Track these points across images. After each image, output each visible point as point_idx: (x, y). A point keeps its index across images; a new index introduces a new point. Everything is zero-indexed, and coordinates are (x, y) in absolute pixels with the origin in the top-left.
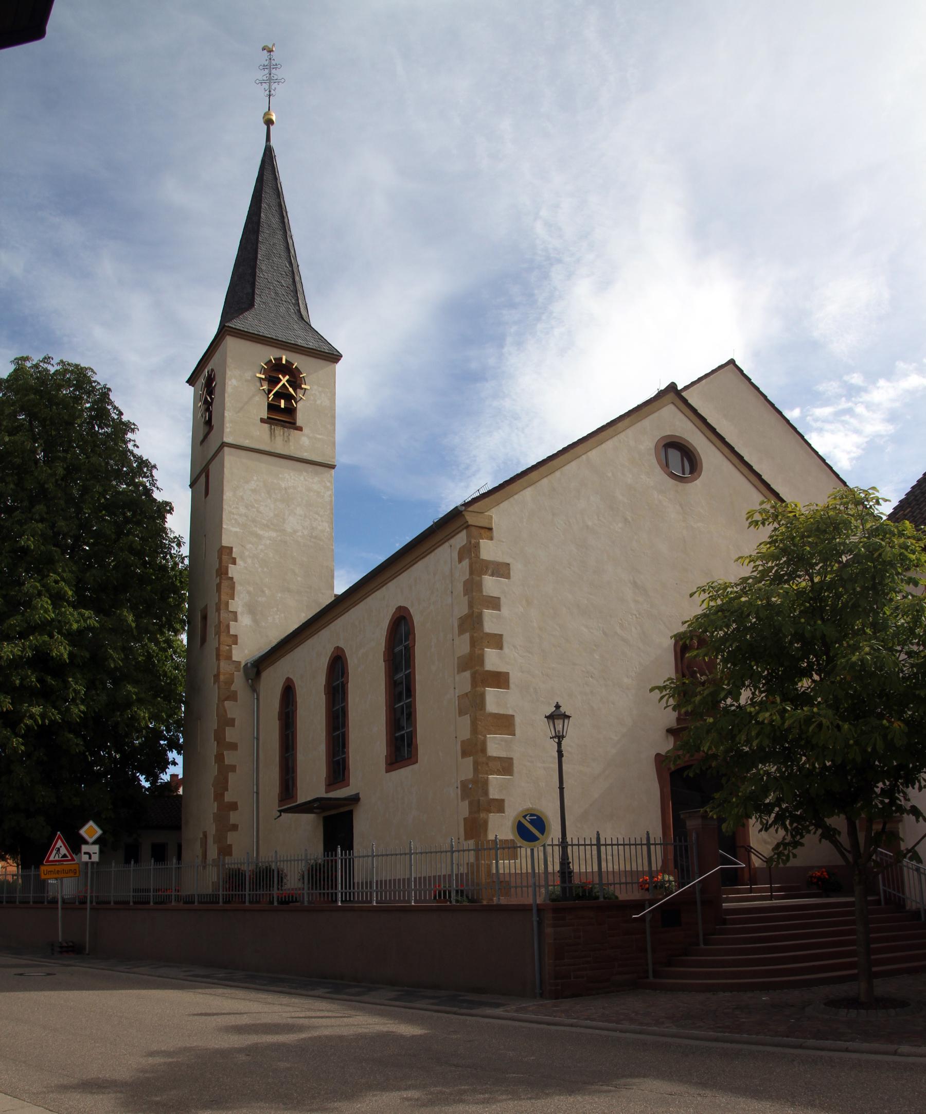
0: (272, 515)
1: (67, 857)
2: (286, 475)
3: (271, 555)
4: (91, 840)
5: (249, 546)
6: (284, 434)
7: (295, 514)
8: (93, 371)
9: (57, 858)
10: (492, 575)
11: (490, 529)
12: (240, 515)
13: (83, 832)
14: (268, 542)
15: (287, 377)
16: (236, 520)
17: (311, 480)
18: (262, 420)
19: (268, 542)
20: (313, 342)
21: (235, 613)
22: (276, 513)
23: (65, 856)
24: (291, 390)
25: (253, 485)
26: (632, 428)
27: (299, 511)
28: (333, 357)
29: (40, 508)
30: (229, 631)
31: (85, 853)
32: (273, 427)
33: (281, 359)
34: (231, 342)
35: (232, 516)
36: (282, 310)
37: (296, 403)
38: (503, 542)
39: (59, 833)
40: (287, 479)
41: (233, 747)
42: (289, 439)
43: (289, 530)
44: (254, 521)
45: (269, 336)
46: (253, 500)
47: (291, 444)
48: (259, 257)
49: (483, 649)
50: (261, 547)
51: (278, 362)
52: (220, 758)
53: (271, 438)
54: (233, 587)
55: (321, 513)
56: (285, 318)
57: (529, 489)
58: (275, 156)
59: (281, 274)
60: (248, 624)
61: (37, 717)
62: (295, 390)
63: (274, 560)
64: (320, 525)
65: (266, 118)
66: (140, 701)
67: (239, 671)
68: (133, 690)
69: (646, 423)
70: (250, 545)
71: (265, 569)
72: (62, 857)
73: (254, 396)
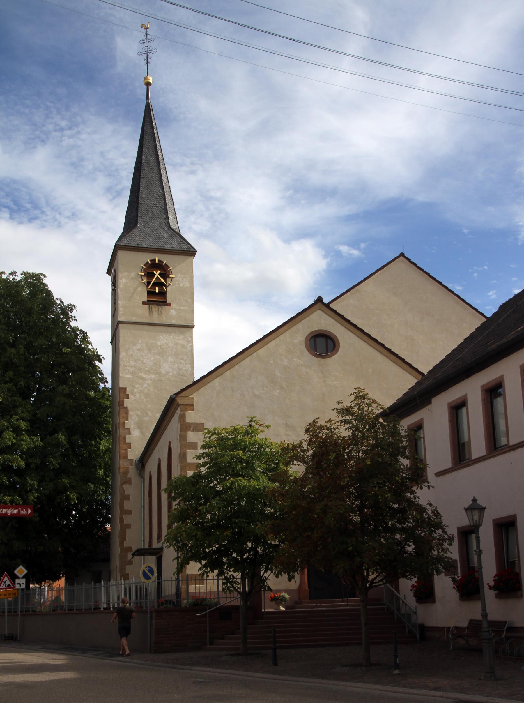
0: (152, 364)
1: (11, 586)
2: (161, 337)
3: (152, 390)
4: (21, 576)
5: (137, 386)
6: (158, 310)
7: (167, 361)
8: (44, 275)
9: (4, 587)
10: (193, 431)
11: (193, 405)
12: (131, 367)
13: (16, 572)
14: (150, 382)
15: (159, 272)
16: (128, 370)
17: (178, 338)
18: (144, 303)
19: (150, 382)
20: (177, 244)
21: (129, 429)
22: (155, 362)
23: (9, 585)
24: (162, 280)
25: (139, 346)
26: (289, 331)
27: (170, 359)
28: (191, 252)
29: (10, 373)
30: (125, 441)
31: (18, 584)
32: (151, 306)
33: (155, 260)
34: (120, 253)
35: (126, 368)
36: (157, 225)
37: (166, 288)
38: (200, 411)
39: (5, 572)
40: (162, 339)
41: (129, 512)
42: (162, 313)
43: (163, 372)
44: (140, 369)
45: (146, 246)
46: (139, 356)
47: (163, 316)
48: (141, 189)
49: (186, 472)
50: (145, 385)
51: (153, 262)
52: (122, 520)
53: (150, 314)
54: (127, 413)
55: (185, 359)
56: (159, 230)
57: (218, 379)
58: (152, 110)
59: (156, 198)
60: (138, 435)
61: (8, 503)
62: (165, 280)
63: (154, 393)
64: (184, 367)
65: (146, 81)
66: (73, 487)
67: (132, 465)
68: (67, 481)
69: (300, 326)
70: (138, 385)
71: (148, 399)
72: (8, 586)
73: (137, 287)
